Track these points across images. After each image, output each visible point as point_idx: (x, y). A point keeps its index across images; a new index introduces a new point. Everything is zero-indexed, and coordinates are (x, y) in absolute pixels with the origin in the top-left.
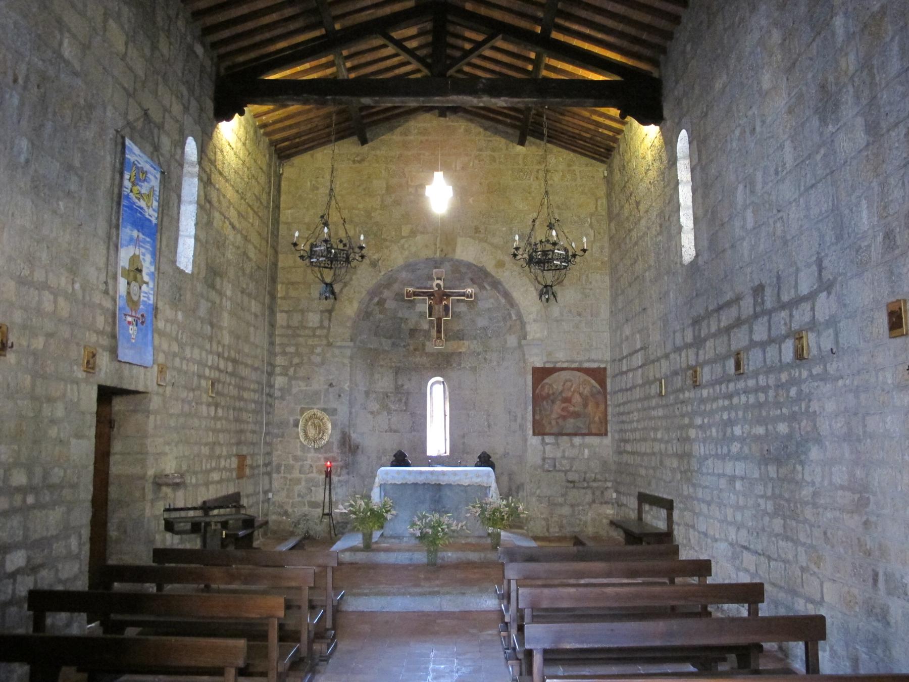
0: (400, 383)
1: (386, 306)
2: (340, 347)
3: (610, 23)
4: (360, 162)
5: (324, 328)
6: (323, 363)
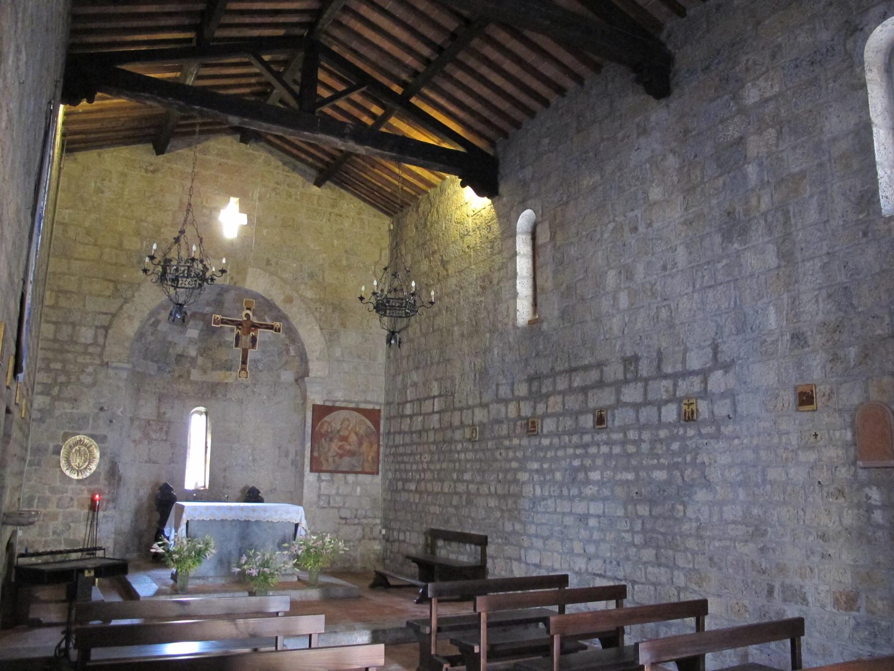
0: (162, 411)
1: (159, 328)
2: (116, 368)
3: (468, 101)
4: (153, 172)
5: (98, 345)
6: (94, 384)
